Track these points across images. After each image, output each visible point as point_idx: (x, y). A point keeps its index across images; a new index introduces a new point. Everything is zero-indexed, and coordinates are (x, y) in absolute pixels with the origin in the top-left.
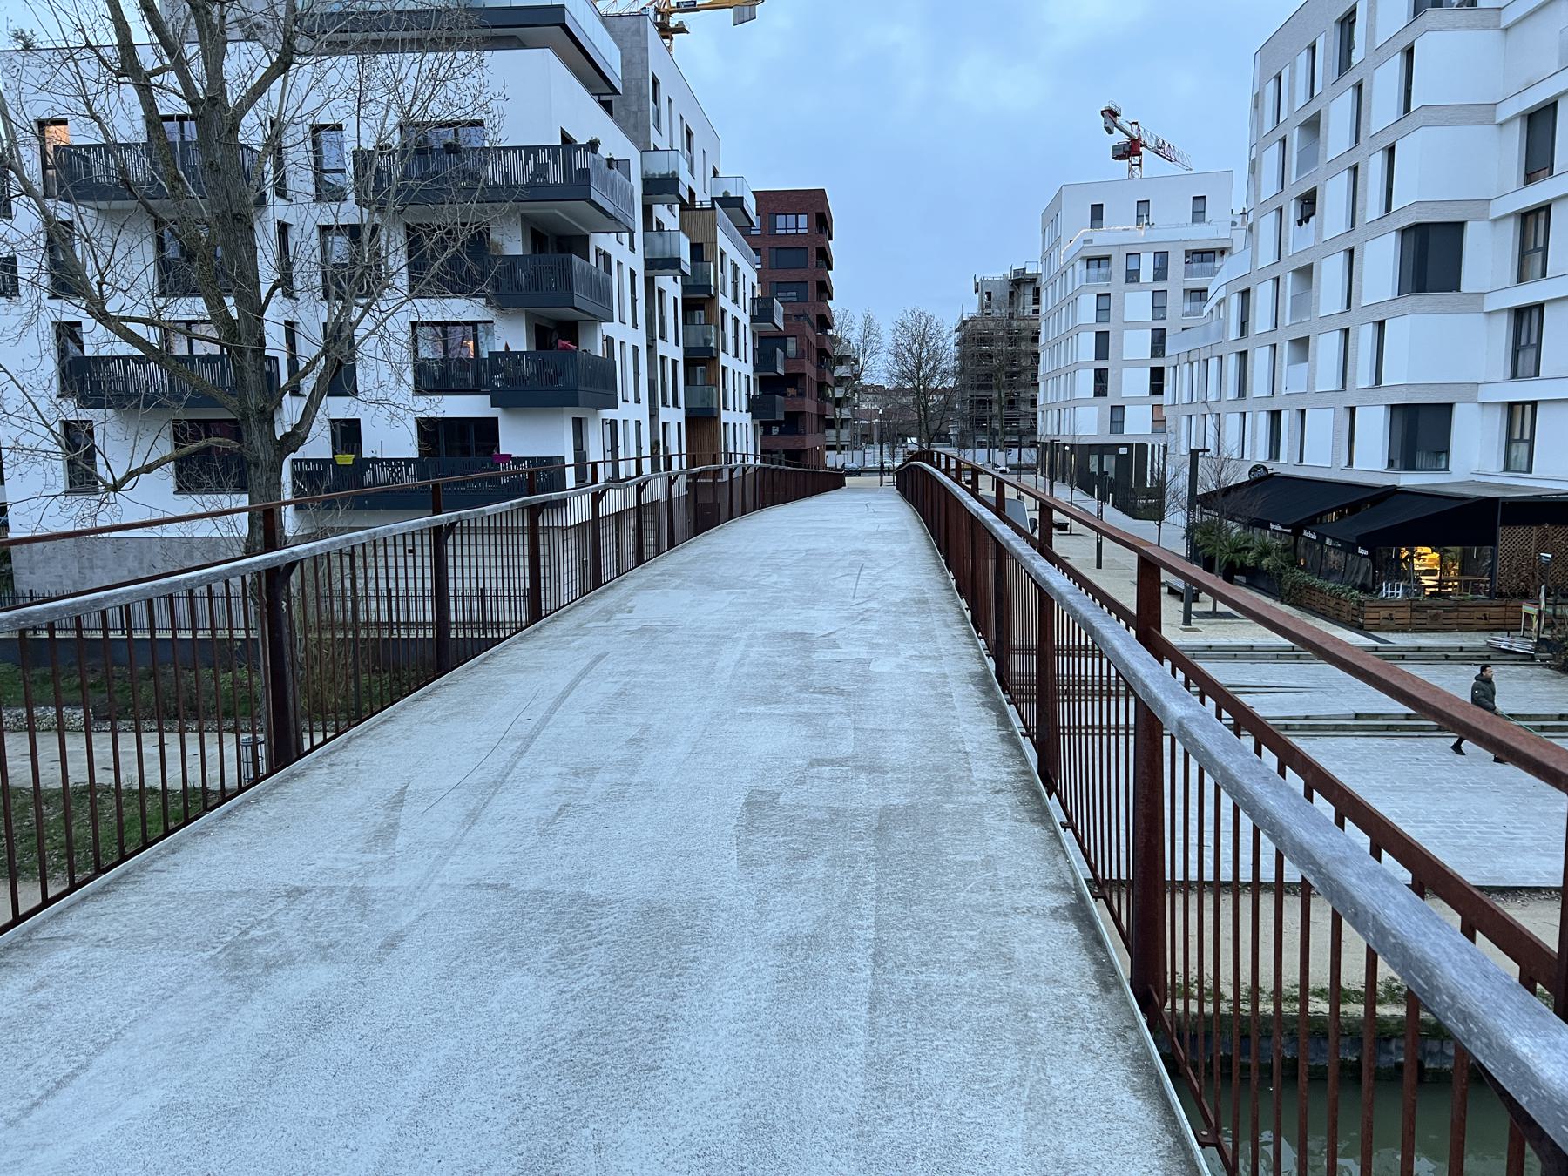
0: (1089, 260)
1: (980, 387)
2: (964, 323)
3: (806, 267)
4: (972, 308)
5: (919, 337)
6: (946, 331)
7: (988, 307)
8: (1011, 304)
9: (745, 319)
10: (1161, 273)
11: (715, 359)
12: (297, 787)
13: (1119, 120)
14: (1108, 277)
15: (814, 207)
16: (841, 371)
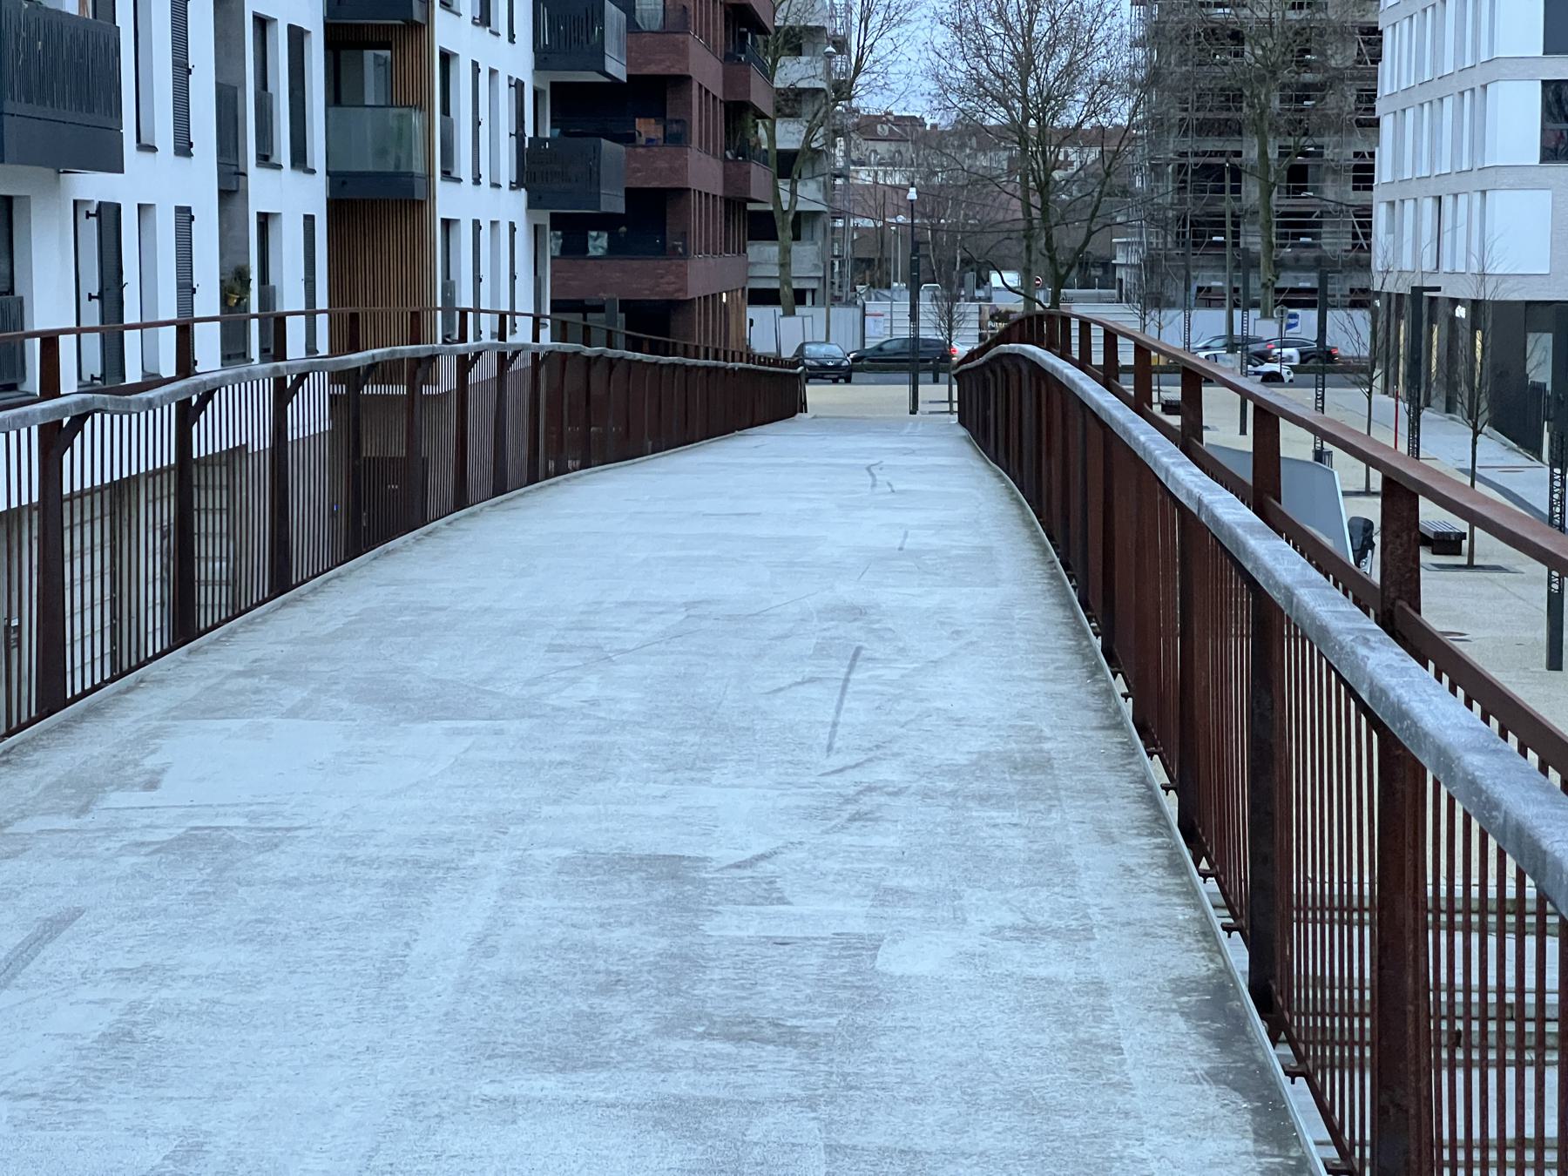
1: (1204, 128)
16: (794, 72)
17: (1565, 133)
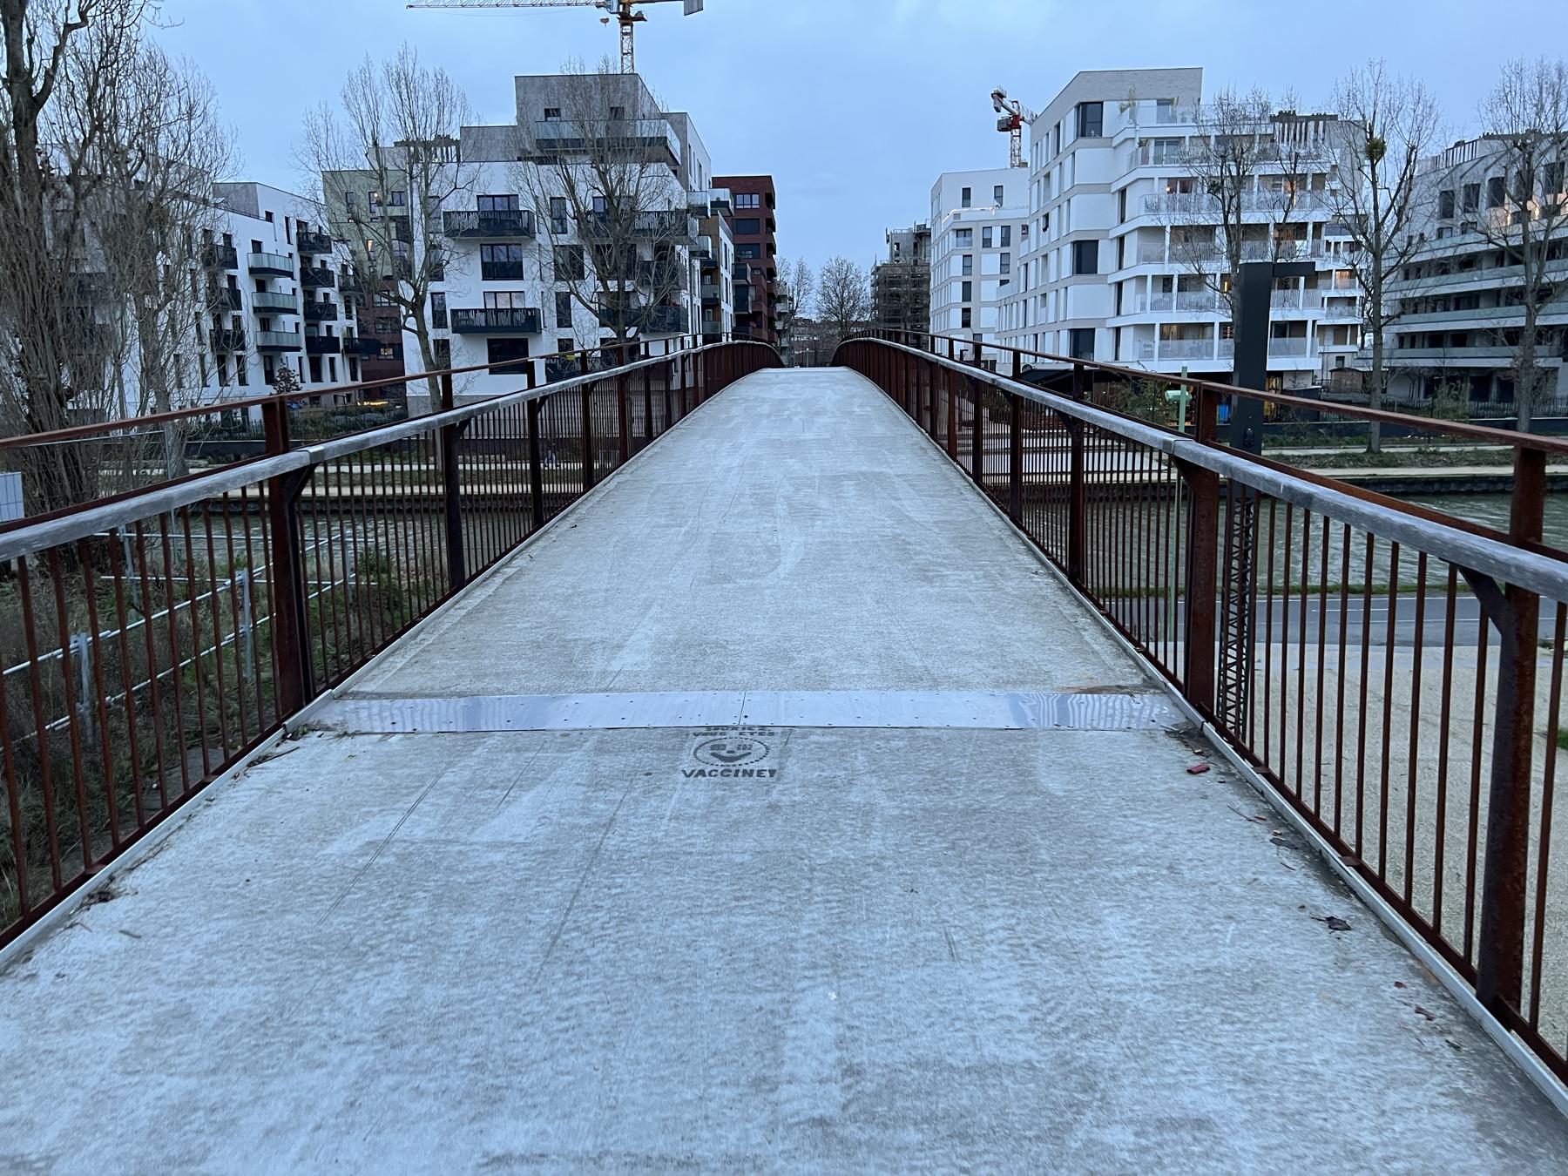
0: (958, 231)
1: (890, 321)
2: (878, 269)
3: (758, 232)
4: (884, 255)
5: (841, 280)
6: (863, 275)
7: (897, 255)
8: (915, 253)
9: (730, 279)
10: (1006, 241)
11: (719, 305)
12: (675, 433)
13: (1005, 101)
14: (970, 244)
15: (763, 188)
16: (780, 308)
17: (1227, 1166)
